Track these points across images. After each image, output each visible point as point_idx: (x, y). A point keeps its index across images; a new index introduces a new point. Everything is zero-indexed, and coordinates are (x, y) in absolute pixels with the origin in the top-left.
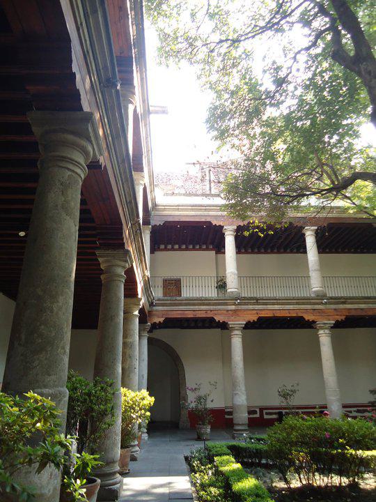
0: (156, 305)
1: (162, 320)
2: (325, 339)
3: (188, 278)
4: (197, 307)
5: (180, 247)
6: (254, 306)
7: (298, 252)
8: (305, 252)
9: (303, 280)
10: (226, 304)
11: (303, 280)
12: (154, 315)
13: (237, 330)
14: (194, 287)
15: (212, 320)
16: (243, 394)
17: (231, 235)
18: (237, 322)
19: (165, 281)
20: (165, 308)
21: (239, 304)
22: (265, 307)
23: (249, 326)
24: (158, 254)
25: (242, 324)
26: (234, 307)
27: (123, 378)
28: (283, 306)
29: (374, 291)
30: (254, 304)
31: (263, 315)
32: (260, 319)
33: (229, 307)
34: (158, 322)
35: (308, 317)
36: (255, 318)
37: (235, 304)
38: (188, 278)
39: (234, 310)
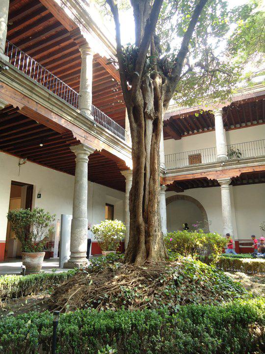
0: (167, 173)
1: (172, 182)
2: (225, 192)
3: (169, 156)
4: (194, 171)
5: (241, 126)
6: (237, 166)
7: (209, 131)
8: (214, 129)
9: (262, 142)
10: (215, 167)
11: (253, 144)
12: (167, 180)
13: (224, 184)
14: (212, 155)
15: (205, 179)
16: (230, 228)
17: (219, 115)
18: (224, 177)
19: (189, 156)
20: (174, 175)
21: (224, 165)
22: (246, 165)
23: (234, 182)
24: (232, 132)
25: (227, 180)
26: (221, 168)
27: (72, 233)
28: (262, 163)
29: (264, 151)
30: (236, 164)
31: (245, 171)
32: (242, 174)
33: (218, 168)
34: (169, 184)
35: (210, 177)
36: (238, 174)
37: (221, 166)
38: (169, 156)
39: (222, 170)
